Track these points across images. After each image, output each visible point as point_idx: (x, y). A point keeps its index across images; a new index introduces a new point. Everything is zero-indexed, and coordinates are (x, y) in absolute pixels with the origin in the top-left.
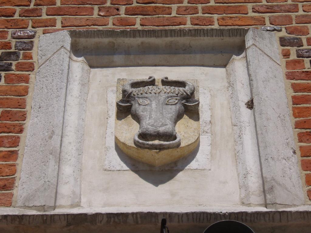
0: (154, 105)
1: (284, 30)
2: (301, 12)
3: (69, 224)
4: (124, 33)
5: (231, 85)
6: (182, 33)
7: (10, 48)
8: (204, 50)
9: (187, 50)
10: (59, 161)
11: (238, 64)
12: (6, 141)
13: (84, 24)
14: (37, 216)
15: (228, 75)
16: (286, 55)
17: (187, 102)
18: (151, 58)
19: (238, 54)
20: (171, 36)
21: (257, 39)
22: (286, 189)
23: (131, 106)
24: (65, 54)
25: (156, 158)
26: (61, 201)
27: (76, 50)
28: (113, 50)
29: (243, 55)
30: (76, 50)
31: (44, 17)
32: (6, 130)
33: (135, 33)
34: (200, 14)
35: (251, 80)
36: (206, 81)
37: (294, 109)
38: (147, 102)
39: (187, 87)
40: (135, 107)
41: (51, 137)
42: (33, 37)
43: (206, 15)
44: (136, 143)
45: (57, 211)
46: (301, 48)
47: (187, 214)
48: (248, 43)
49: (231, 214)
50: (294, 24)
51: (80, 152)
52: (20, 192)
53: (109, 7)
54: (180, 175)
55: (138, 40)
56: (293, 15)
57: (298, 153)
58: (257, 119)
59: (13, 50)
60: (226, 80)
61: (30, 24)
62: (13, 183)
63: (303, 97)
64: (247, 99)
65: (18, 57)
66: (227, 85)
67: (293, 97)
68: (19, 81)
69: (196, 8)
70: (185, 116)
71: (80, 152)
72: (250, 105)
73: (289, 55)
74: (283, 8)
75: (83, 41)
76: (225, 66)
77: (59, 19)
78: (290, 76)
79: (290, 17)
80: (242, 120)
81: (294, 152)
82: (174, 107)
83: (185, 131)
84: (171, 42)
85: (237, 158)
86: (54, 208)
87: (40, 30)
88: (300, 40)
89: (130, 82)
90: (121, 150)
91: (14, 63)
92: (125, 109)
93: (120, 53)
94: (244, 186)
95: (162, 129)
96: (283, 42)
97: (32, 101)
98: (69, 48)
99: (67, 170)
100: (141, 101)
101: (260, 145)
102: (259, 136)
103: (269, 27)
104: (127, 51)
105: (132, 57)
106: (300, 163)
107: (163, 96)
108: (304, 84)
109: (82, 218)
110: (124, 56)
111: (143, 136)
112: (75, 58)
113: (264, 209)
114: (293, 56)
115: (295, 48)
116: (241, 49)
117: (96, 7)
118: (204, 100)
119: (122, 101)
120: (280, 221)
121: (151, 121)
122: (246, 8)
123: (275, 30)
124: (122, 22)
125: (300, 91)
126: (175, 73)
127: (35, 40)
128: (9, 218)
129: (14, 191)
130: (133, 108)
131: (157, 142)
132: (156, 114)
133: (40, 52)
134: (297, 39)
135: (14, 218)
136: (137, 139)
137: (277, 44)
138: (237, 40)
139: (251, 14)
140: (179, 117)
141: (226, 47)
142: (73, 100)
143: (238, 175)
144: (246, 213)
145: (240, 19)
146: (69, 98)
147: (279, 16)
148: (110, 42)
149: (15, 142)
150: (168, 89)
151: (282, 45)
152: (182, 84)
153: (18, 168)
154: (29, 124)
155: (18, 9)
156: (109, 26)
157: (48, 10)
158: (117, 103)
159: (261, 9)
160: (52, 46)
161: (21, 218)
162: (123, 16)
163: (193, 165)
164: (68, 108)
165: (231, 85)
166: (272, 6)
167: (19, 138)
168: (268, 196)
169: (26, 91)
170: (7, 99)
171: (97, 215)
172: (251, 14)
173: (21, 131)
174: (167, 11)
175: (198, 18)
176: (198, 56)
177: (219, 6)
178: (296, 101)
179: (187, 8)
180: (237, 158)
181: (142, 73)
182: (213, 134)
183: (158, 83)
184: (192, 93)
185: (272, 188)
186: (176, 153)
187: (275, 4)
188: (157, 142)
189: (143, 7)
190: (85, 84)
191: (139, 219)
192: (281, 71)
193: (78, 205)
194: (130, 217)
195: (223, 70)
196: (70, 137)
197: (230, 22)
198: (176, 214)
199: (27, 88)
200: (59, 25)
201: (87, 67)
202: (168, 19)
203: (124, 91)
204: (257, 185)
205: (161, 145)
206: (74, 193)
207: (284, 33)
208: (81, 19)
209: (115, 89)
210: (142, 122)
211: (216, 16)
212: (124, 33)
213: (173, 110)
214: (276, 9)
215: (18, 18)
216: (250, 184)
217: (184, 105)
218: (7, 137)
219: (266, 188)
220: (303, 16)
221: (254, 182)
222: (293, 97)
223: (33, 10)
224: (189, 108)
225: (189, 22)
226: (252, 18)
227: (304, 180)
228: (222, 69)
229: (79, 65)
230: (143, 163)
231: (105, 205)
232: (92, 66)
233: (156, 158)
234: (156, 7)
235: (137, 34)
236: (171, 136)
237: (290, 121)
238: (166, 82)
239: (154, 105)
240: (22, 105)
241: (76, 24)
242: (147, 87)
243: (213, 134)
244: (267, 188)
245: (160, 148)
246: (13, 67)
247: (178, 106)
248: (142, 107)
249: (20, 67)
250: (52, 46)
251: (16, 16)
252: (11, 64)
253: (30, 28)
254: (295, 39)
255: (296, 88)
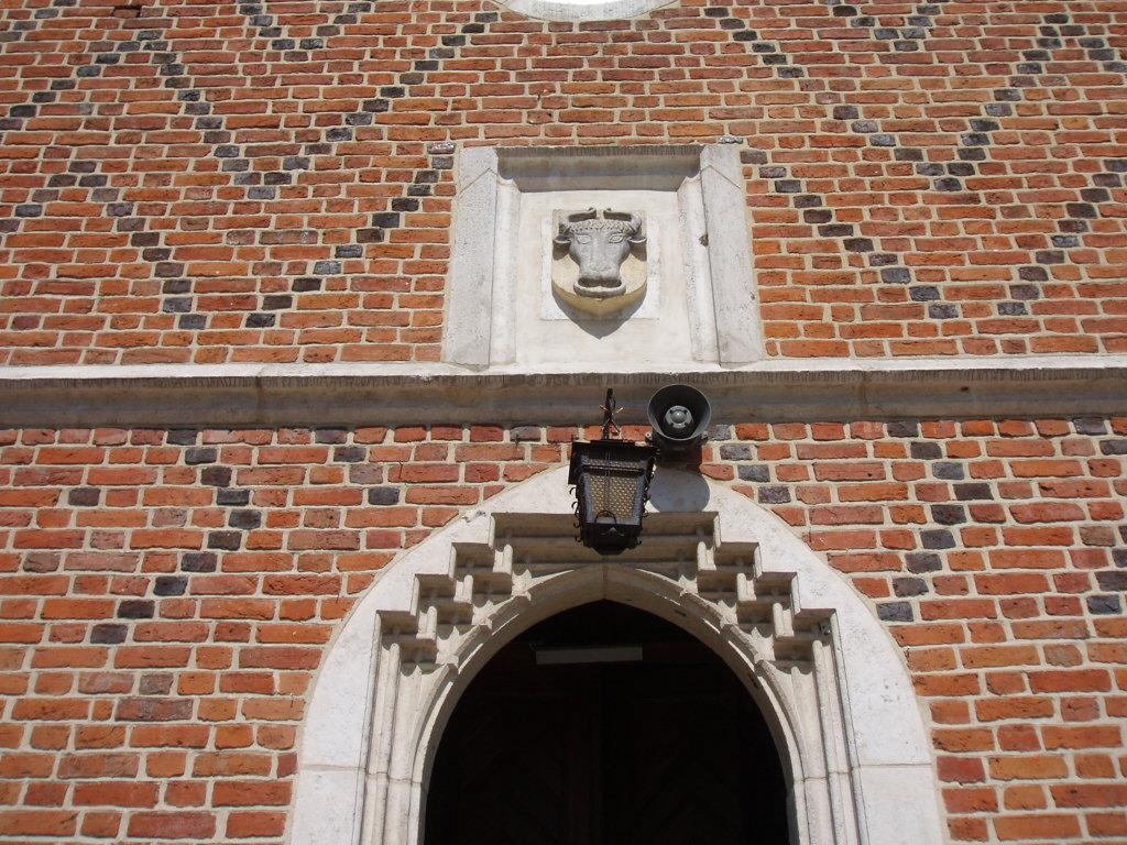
0: (595, 243)
1: (745, 141)
2: (766, 118)
3: (505, 386)
4: (559, 151)
5: (683, 214)
6: (624, 150)
7: (427, 166)
8: (652, 171)
9: (633, 170)
10: (491, 313)
11: (691, 187)
12: (429, 284)
13: (510, 134)
14: (471, 377)
15: (680, 200)
16: (748, 174)
17: (633, 238)
18: (591, 180)
19: (692, 176)
20: (614, 154)
21: (714, 158)
22: (742, 343)
23: (569, 244)
24: (493, 177)
25: (598, 307)
26: (495, 358)
27: (504, 171)
28: (546, 171)
29: (698, 176)
30: (504, 171)
31: (464, 125)
32: (429, 270)
33: (572, 151)
34: (647, 121)
35: (706, 211)
36: (649, 206)
37: (754, 243)
38: (588, 240)
39: (633, 221)
40: (574, 245)
41: (481, 284)
42: (452, 151)
43: (655, 122)
44: (575, 289)
45: (492, 371)
46: (764, 165)
47: (633, 375)
48: (704, 164)
49: (681, 376)
50: (758, 135)
51: (513, 298)
52: (450, 343)
53: (540, 112)
54: (625, 324)
55: (577, 159)
56: (757, 121)
57: (758, 298)
58: (712, 261)
59: (430, 169)
60: (677, 208)
61: (325, 205)
62: (441, 334)
63: (765, 228)
64: (701, 233)
65: (436, 177)
66: (678, 214)
67: (755, 229)
68: (440, 209)
69: (643, 113)
70: (631, 256)
71: (513, 298)
72: (705, 241)
73: (751, 175)
74: (745, 113)
75: (511, 160)
76: (676, 190)
77: (481, 126)
78: (751, 202)
79: (753, 125)
80: (695, 258)
81: (753, 298)
82: (617, 246)
83: (631, 274)
84: (614, 161)
85: (689, 305)
86: (488, 367)
87: (460, 142)
88: (764, 154)
89: (568, 215)
90: (558, 294)
91: (433, 185)
92: (563, 248)
93: (554, 175)
94: (695, 339)
95: (605, 274)
96: (745, 158)
97: (458, 232)
98: (495, 169)
99: (500, 320)
100: (580, 238)
101: (716, 292)
102: (714, 280)
103: (728, 136)
104: (563, 172)
105: (569, 178)
106: (759, 310)
107: (606, 232)
108: (765, 212)
109: (519, 380)
110: (559, 178)
111: (584, 281)
112: (503, 181)
113: (717, 369)
114: (756, 177)
115: (759, 165)
116: (694, 169)
117: (525, 112)
118: (651, 234)
119: (559, 238)
120: (735, 381)
121: (593, 264)
122: (700, 112)
123: (735, 142)
124: (557, 132)
125: (762, 220)
126: (618, 200)
127: (455, 155)
128: (440, 380)
129: (442, 344)
130: (572, 247)
131: (599, 289)
132: (598, 254)
133: (462, 173)
134: (760, 153)
135: (445, 379)
136: (577, 285)
137: (737, 160)
138: (690, 158)
139: (708, 121)
140: (624, 257)
141: (678, 166)
142: (503, 235)
143: (690, 325)
144: (698, 374)
145: (695, 127)
146: (498, 231)
147: (740, 123)
148: (542, 161)
149: (439, 285)
150: (612, 223)
151: (743, 162)
152: (627, 217)
153: (444, 315)
154: (454, 262)
155: (433, 115)
156: (458, 484)
157: (468, 115)
158: (554, 242)
159: (719, 115)
160: (474, 163)
161: (454, 379)
162: (557, 123)
163: (639, 313)
164: (498, 244)
165: (683, 214)
166: (733, 111)
167: (443, 279)
168: (723, 354)
169: (447, 222)
170: (427, 231)
171: (536, 376)
172: (708, 121)
173: (445, 271)
174: (516, 40)
175: (644, 127)
176: (646, 178)
177: (671, 111)
178: (757, 233)
179: (632, 114)
180: (689, 305)
181: (582, 200)
182: (662, 275)
183: (600, 215)
184: (639, 228)
185: (726, 345)
186: (620, 301)
187: (736, 107)
188: (599, 289)
189: (580, 112)
190: (515, 214)
191: (581, 382)
192: (740, 196)
193: (512, 361)
194: (572, 378)
195: (673, 194)
196: (502, 280)
197: (683, 132)
198: (621, 375)
199: (449, 217)
200: (481, 137)
201: (517, 192)
202: (609, 128)
203: (561, 226)
204: (710, 338)
205: (605, 293)
206: (508, 346)
207: (745, 147)
208: (506, 128)
209: (550, 219)
210: (582, 264)
211: (666, 124)
212: (559, 151)
213: (618, 248)
214: (737, 114)
215: (434, 126)
216: (703, 337)
217: (630, 243)
218: (431, 278)
219: (720, 345)
220: (768, 123)
221: (707, 335)
222: (755, 229)
223: (451, 117)
224: (635, 246)
225: (634, 132)
226: (709, 126)
227: (763, 330)
228: (673, 193)
229: (508, 188)
230: (585, 312)
231: (544, 361)
232: (522, 190)
233: (598, 307)
234: (595, 112)
235: (575, 152)
236: (615, 282)
237: (749, 258)
238: (609, 215)
239: (595, 243)
240: (444, 239)
241: (502, 134)
242: (587, 221)
243: (662, 275)
244: (721, 344)
245: (603, 296)
246: (432, 191)
247: (623, 245)
248: (582, 246)
249: (440, 190)
250: (474, 163)
251: (431, 125)
252: (429, 187)
253: (448, 139)
254: (757, 153)
255: (758, 217)
